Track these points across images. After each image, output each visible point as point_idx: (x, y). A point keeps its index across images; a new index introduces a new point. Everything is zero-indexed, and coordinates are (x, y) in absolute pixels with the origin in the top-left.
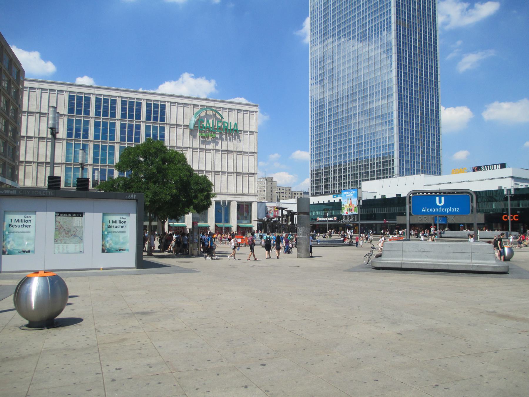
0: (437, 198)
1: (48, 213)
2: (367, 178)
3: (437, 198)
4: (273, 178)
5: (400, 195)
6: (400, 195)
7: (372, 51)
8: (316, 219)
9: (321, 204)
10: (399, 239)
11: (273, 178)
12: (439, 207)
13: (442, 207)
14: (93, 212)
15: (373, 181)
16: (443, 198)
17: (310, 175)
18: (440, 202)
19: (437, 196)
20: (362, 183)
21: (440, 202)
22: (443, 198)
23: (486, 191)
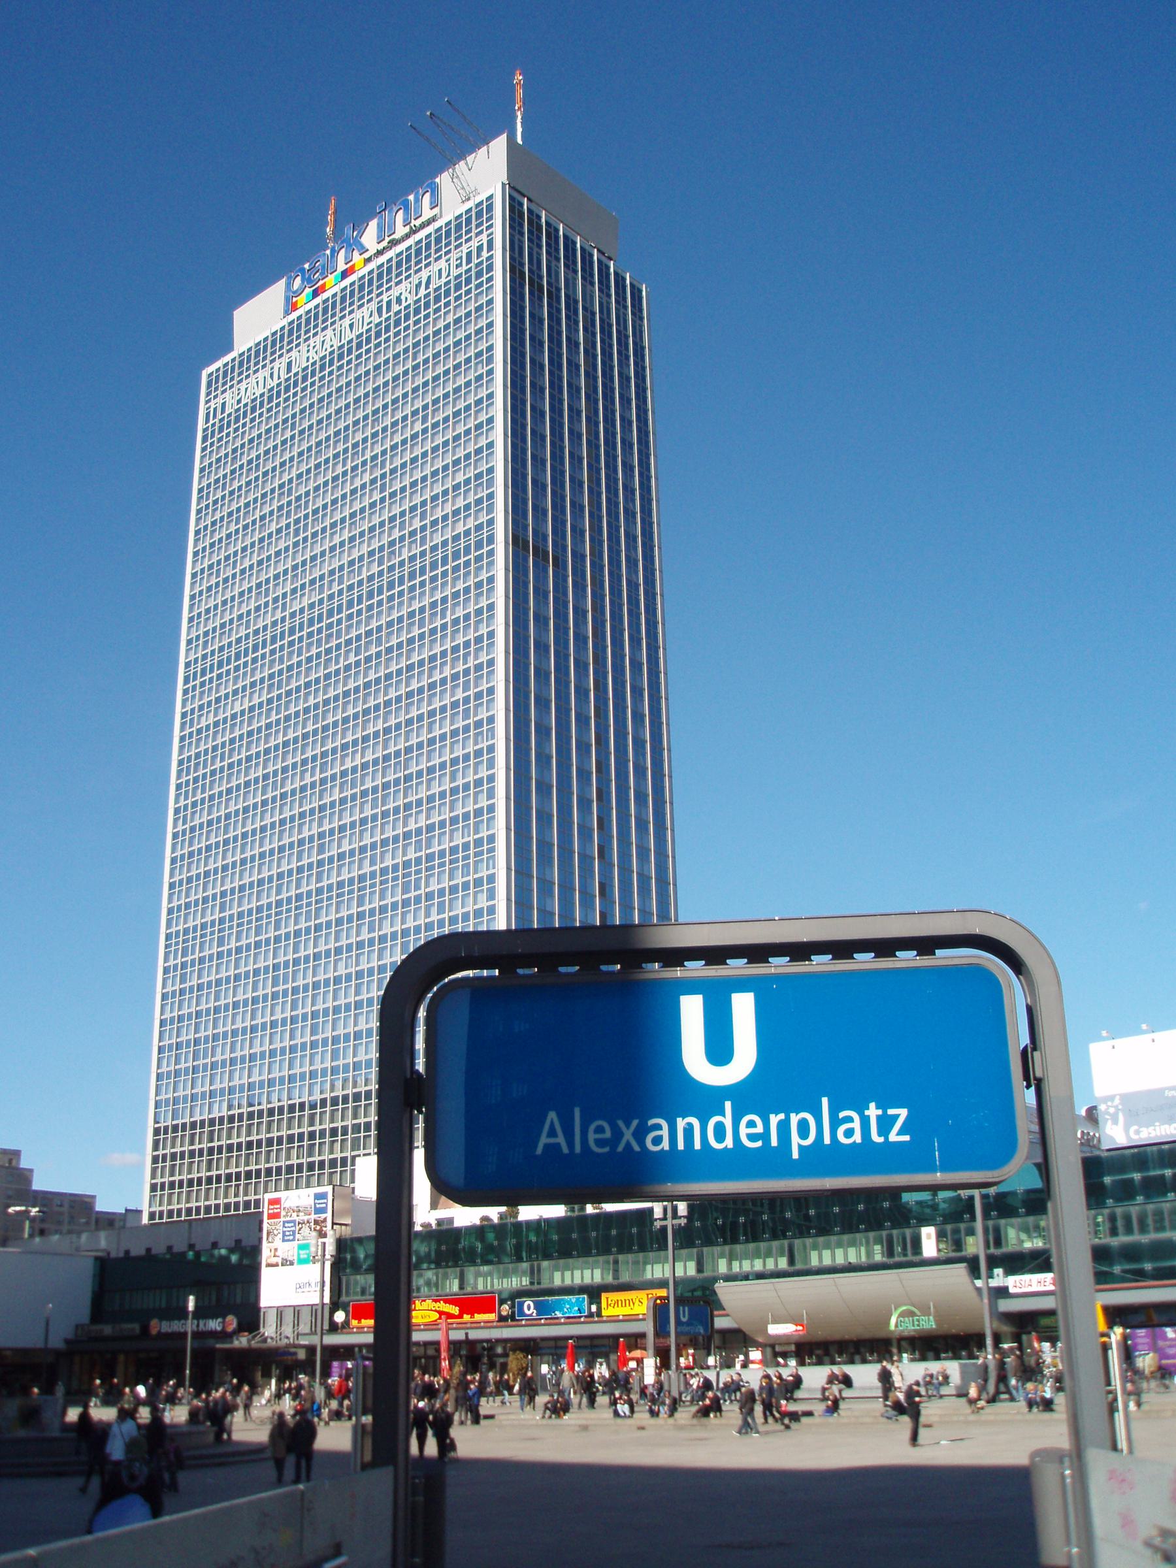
3: (692, 1009)
4: (17, 1153)
11: (17, 1153)
13: (745, 1097)
16: (743, 1006)
17: (149, 1160)
18: (719, 1049)
21: (719, 1049)
22: (743, 1006)
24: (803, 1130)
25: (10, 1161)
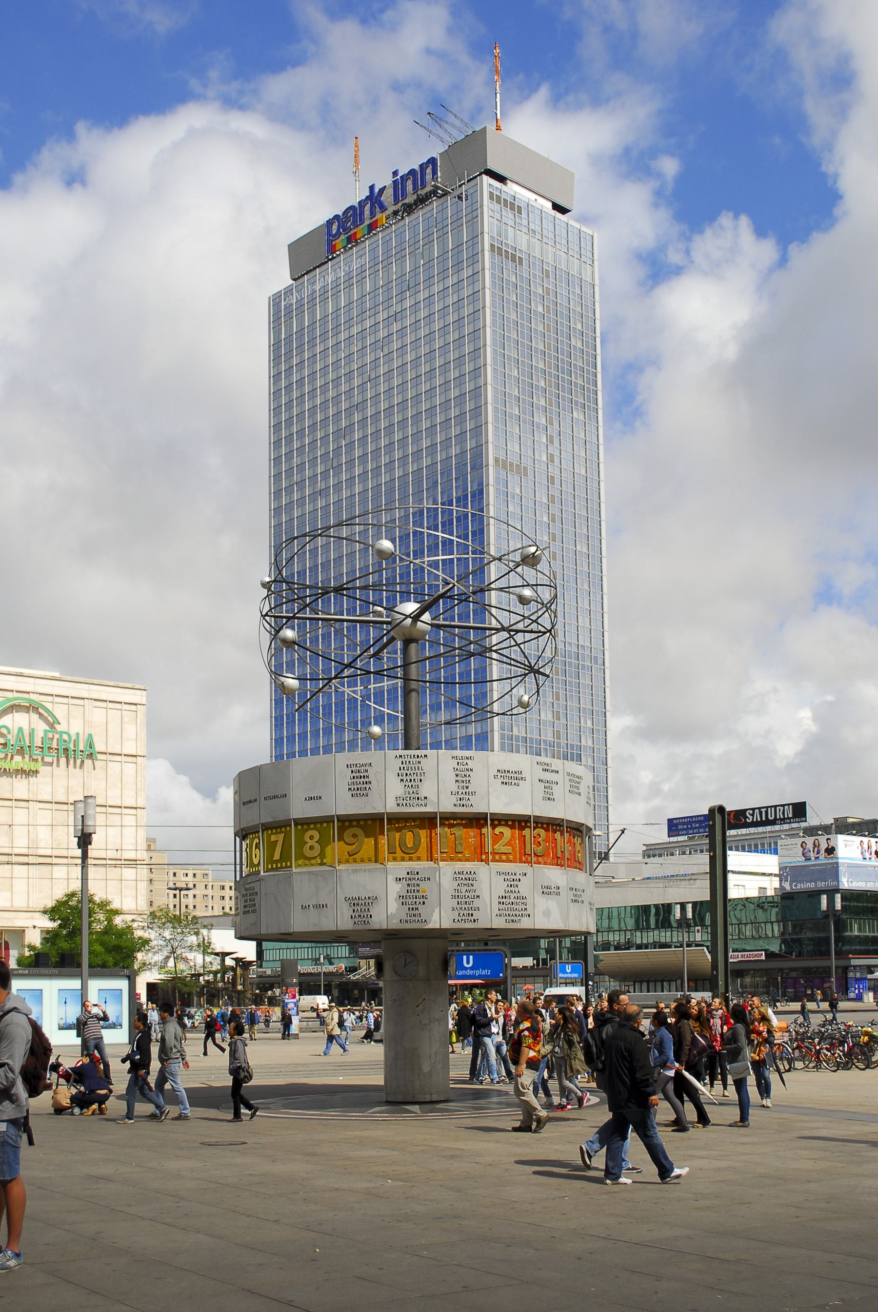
0: (465, 957)
3: (465, 957)
12: (466, 969)
13: (471, 968)
16: (471, 957)
18: (468, 963)
21: (468, 963)
22: (471, 957)
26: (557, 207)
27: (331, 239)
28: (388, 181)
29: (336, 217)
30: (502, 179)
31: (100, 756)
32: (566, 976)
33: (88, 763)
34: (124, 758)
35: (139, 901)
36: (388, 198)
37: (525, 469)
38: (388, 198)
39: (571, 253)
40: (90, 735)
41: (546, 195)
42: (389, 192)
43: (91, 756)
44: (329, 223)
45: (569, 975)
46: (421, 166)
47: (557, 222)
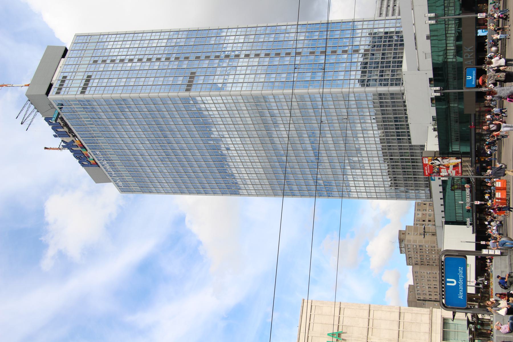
0: (448, 284)
1: (438, 146)
2: (402, 104)
3: (448, 284)
5: (430, 80)
6: (430, 80)
7: (130, 107)
8: (468, 211)
9: (444, 202)
10: (492, 272)
12: (458, 284)
13: (458, 280)
14: (439, 145)
15: (410, 126)
16: (448, 280)
18: (453, 282)
19: (446, 284)
20: (414, 143)
21: (453, 282)
22: (448, 280)
23: (431, 47)
24: (461, 276)
25: (403, 234)
26: (64, 56)
27: (90, 164)
28: (59, 140)
29: (79, 162)
30: (51, 85)
31: (340, 330)
32: (474, 79)
33: (343, 336)
34: (341, 316)
35: (424, 313)
36: (68, 140)
37: (192, 73)
38: (68, 140)
39: (85, 48)
40: (328, 334)
41: (58, 62)
42: (65, 139)
43: (339, 335)
44: (83, 165)
45: (474, 77)
46: (50, 125)
47: (70, 56)
